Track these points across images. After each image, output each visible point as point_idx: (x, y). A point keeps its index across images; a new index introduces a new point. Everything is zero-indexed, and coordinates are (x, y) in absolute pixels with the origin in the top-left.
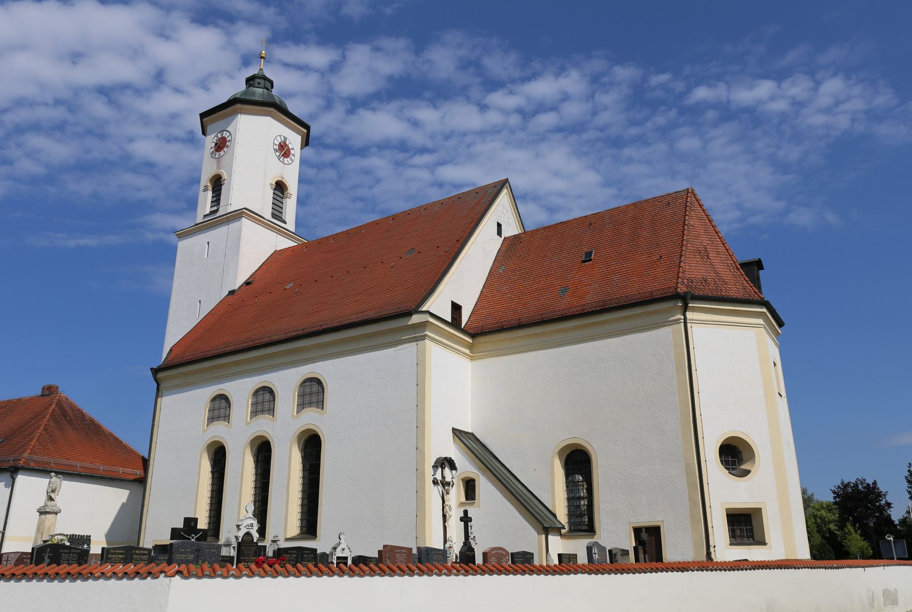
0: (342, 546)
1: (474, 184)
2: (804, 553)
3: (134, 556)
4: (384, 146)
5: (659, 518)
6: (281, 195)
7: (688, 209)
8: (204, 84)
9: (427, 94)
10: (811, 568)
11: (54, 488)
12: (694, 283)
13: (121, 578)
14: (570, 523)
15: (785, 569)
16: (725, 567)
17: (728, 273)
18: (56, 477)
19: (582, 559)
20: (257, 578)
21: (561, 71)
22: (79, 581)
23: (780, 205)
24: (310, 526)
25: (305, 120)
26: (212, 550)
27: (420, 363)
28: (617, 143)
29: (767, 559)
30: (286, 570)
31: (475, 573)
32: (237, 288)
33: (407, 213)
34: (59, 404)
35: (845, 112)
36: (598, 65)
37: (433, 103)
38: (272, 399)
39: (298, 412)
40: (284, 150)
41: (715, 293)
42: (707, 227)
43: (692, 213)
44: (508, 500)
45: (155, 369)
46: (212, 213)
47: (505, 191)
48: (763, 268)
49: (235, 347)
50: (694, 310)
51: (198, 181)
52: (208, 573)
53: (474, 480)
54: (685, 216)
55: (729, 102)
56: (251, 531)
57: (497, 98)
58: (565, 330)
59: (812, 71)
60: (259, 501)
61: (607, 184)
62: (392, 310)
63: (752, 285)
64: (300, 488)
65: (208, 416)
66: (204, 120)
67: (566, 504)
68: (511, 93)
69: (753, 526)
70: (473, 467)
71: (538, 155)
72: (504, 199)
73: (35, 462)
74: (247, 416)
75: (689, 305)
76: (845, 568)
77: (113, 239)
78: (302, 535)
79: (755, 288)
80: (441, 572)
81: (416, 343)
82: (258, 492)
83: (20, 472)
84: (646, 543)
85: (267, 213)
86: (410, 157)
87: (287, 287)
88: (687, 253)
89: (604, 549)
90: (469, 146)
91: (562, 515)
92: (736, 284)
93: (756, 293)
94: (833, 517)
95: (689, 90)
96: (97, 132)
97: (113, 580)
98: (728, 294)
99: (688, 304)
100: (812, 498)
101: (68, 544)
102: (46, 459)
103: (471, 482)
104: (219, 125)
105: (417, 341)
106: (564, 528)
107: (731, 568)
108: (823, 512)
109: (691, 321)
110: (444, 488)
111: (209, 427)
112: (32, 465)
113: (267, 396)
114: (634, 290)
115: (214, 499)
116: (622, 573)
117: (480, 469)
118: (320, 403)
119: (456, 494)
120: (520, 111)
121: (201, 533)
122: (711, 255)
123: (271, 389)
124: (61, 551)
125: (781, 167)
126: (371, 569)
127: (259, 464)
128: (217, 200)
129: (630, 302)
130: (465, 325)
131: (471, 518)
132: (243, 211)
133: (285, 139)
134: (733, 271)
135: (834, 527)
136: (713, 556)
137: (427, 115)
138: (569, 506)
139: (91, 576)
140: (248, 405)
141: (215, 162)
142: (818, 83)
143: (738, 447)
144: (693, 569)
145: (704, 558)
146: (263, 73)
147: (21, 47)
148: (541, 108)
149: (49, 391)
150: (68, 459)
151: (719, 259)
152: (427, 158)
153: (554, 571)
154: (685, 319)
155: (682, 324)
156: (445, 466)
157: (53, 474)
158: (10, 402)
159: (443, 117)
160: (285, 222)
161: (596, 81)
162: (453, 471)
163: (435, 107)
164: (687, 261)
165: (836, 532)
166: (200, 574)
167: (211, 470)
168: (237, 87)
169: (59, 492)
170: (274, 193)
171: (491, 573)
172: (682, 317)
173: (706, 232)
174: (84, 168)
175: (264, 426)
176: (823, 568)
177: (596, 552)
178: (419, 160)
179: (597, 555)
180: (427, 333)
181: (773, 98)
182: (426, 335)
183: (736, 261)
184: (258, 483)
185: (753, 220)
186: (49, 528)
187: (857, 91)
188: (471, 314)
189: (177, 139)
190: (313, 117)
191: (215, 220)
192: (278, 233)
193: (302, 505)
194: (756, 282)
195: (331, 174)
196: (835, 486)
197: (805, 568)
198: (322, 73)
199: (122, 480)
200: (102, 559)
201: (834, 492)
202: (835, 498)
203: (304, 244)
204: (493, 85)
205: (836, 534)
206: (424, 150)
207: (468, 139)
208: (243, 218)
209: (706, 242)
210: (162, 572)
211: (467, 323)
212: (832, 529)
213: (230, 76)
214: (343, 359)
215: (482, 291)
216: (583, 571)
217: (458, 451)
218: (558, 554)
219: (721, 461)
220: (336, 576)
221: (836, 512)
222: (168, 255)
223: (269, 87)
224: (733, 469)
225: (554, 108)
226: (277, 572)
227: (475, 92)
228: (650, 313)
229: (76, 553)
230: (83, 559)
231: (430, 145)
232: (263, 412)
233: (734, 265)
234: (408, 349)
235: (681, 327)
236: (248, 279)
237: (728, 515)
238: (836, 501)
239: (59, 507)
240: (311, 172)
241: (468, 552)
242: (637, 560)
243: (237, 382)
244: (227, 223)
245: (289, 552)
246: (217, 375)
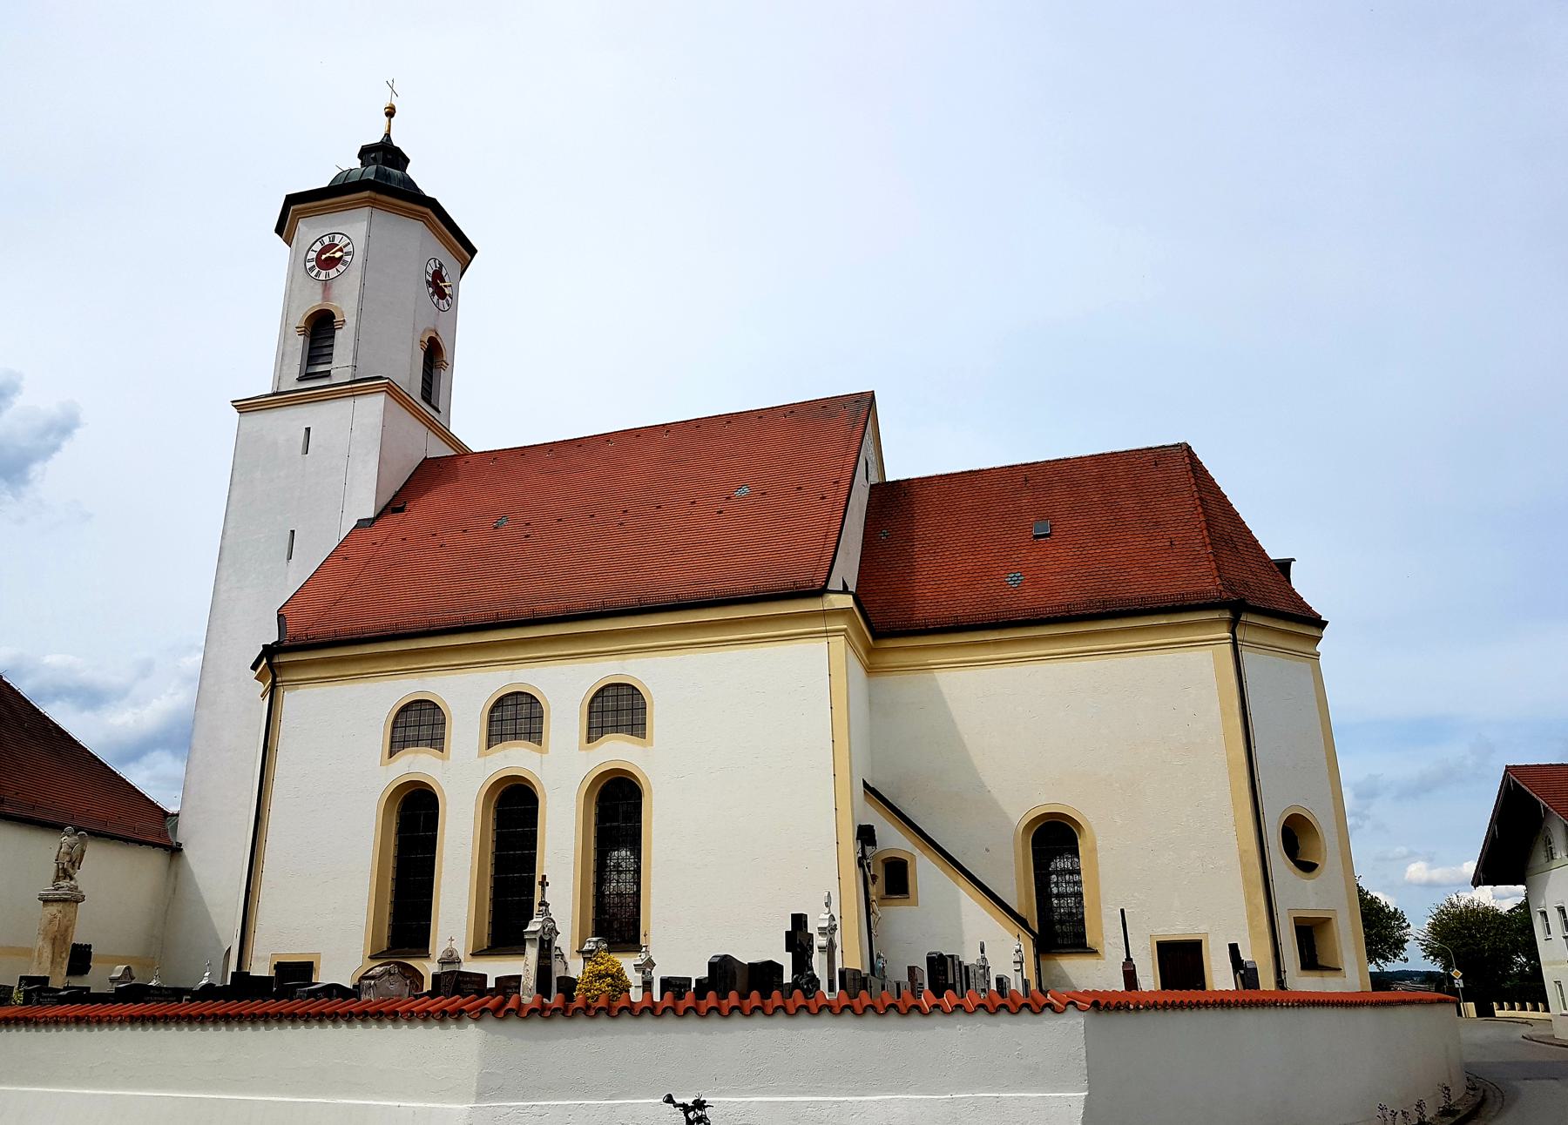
5: (1107, 956)
19: (528, 994)
50: (1247, 624)
99: (1241, 616)
160: (439, 412)
239: (81, 892)
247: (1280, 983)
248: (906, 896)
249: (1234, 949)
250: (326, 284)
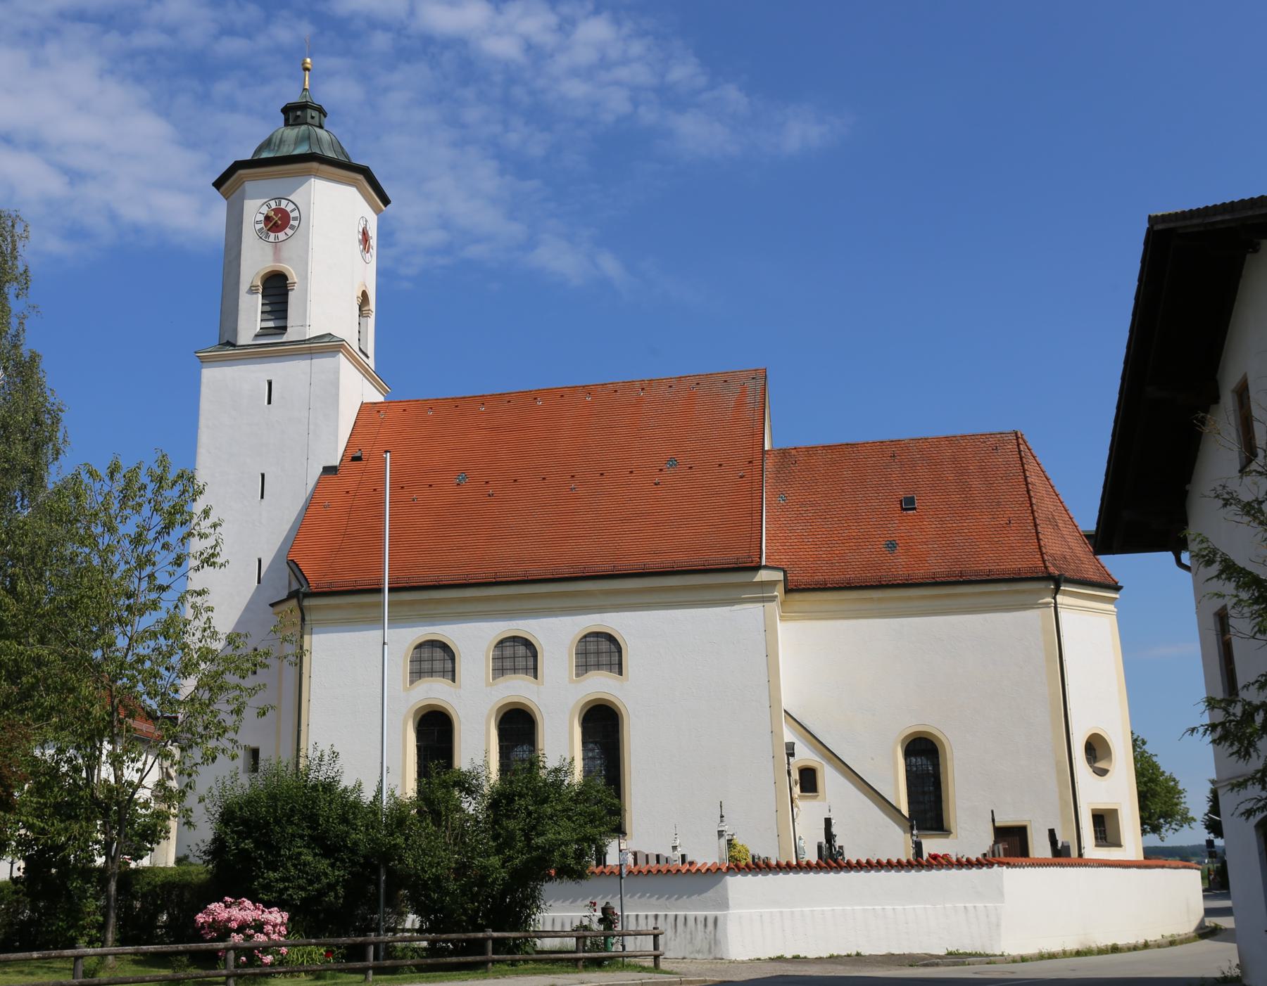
35: (618, 83)
50: (1066, 593)
70: (811, 753)
74: (487, 674)
75: (1062, 588)
81: (763, 604)
105: (763, 602)
132: (343, 344)
141: (269, 249)
155: (1053, 608)
160: (368, 357)
172: (1053, 601)
187: (637, 48)
192: (364, 375)
205: (247, 849)
208: (341, 354)
209: (1052, 508)
214: (649, 612)
217: (790, 734)
228: (1017, 592)
235: (1051, 611)
244: (309, 356)
247: (1080, 855)
248: (815, 794)
249: (1052, 833)
250: (276, 246)
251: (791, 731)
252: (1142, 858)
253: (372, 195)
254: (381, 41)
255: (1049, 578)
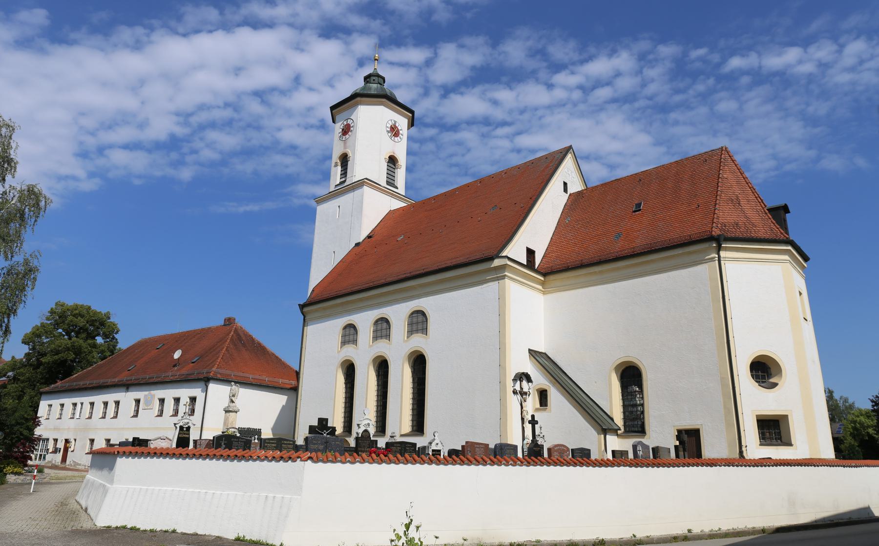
0: (436, 442)
1: (545, 149)
2: (828, 452)
3: (283, 445)
4: (471, 122)
6: (394, 167)
7: (722, 164)
8: (330, 83)
9: (504, 79)
10: (830, 466)
11: (234, 393)
12: (727, 227)
13: (271, 461)
14: (625, 425)
15: (805, 466)
16: (749, 463)
17: (757, 217)
18: (235, 385)
20: (367, 464)
21: (613, 53)
22: (243, 461)
23: (812, 153)
24: (418, 426)
25: (408, 106)
26: (337, 443)
27: (501, 298)
28: (664, 109)
29: (792, 458)
30: (389, 458)
31: (542, 464)
32: (361, 241)
33: (491, 177)
34: (236, 330)
35: (869, 69)
36: (644, 45)
37: (509, 86)
38: (388, 327)
39: (408, 337)
40: (394, 131)
41: (745, 235)
42: (738, 179)
43: (726, 167)
44: (574, 407)
45: (302, 305)
46: (341, 183)
47: (569, 157)
48: (789, 212)
49: (359, 287)
50: (727, 249)
51: (330, 158)
52: (331, 459)
53: (546, 391)
54: (720, 170)
55: (760, 67)
56: (368, 428)
57: (561, 78)
58: (618, 269)
59: (835, 36)
60: (380, 406)
61: (658, 143)
62: (478, 256)
63: (779, 227)
64: (411, 396)
65: (341, 341)
66: (333, 112)
67: (622, 410)
68: (573, 73)
69: (781, 429)
71: (598, 123)
72: (569, 161)
73: (220, 374)
75: (723, 245)
76: (864, 467)
77: (269, 205)
78: (413, 432)
79: (781, 230)
80: (508, 463)
82: (379, 399)
83: (211, 381)
84: (685, 443)
85: (383, 182)
86: (494, 130)
87: (399, 239)
88: (721, 202)
89: (647, 447)
90: (540, 118)
91: (619, 419)
92: (764, 226)
93: (781, 233)
94: (872, 423)
95: (724, 60)
96: (255, 125)
97: (266, 462)
98: (757, 235)
99: (722, 244)
100: (853, 406)
101: (238, 435)
102: (228, 372)
103: (544, 392)
104: (344, 115)
105: (498, 280)
106: (620, 430)
107: (755, 464)
108: (862, 419)
109: (724, 259)
110: (522, 397)
111: (342, 348)
112: (219, 376)
113: (385, 325)
114: (677, 233)
115: (347, 404)
116: (658, 467)
117: (551, 382)
118: (425, 330)
119: (532, 402)
120: (581, 87)
121: (331, 429)
122: (742, 203)
123: (423, 312)
124: (232, 440)
125: (811, 121)
126: (454, 460)
127: (380, 377)
128: (344, 173)
129: (672, 244)
130: (539, 266)
131: (537, 421)
133: (395, 122)
134: (761, 215)
135: (873, 432)
136: (745, 454)
137: (505, 95)
138: (624, 413)
139: (250, 458)
140: (370, 331)
141: (342, 143)
142: (842, 47)
143: (767, 363)
144: (720, 465)
145: (737, 456)
146: (377, 72)
147: (200, 67)
148: (598, 83)
149: (229, 321)
150: (243, 373)
151: (749, 205)
152: (506, 130)
153: (600, 464)
154: (719, 257)
155: (717, 262)
156: (523, 379)
157: (233, 383)
158: (203, 330)
159: (518, 96)
161: (643, 58)
162: (530, 383)
163: (511, 89)
164: (721, 209)
165: (875, 436)
166: (325, 460)
167: (344, 382)
168: (357, 84)
169: (237, 396)
170: (388, 165)
171: (556, 464)
172: (717, 256)
173: (738, 183)
174: (247, 153)
175: (382, 348)
176: (841, 466)
177: (641, 449)
178: (501, 131)
179: (641, 452)
180: (506, 273)
181: (800, 62)
182: (505, 275)
183: (764, 207)
184: (380, 392)
185: (788, 167)
186: (232, 422)
188: (543, 257)
189: (312, 126)
190: (414, 102)
191: (344, 189)
193: (413, 409)
194: (783, 224)
195: (431, 146)
196: (873, 396)
197: (824, 466)
198: (420, 68)
199: (282, 388)
200: (261, 447)
201: (872, 401)
202: (873, 406)
203: (412, 204)
204: (558, 67)
205: (875, 437)
206: (504, 124)
207: (539, 113)
210: (298, 457)
211: (540, 264)
212: (871, 433)
213: (350, 75)
215: (552, 238)
216: (625, 464)
218: (612, 451)
219: (752, 376)
220: (434, 464)
221: (875, 418)
222: (310, 216)
223: (382, 82)
224: (763, 382)
225: (608, 83)
226: (382, 460)
227: (543, 75)
228: (690, 253)
229: (242, 442)
230: (247, 447)
231: (509, 119)
232: (381, 337)
233: (763, 211)
234: (493, 286)
236: (369, 234)
237: (758, 421)
238: (874, 409)
240: (416, 146)
241: (535, 447)
242: (677, 456)
243: (361, 314)
244: (353, 191)
245: (395, 445)
246: (347, 309)
251: (533, 366)
252: (834, 457)
253: (396, 108)
254: (745, 80)
255: (711, 239)
